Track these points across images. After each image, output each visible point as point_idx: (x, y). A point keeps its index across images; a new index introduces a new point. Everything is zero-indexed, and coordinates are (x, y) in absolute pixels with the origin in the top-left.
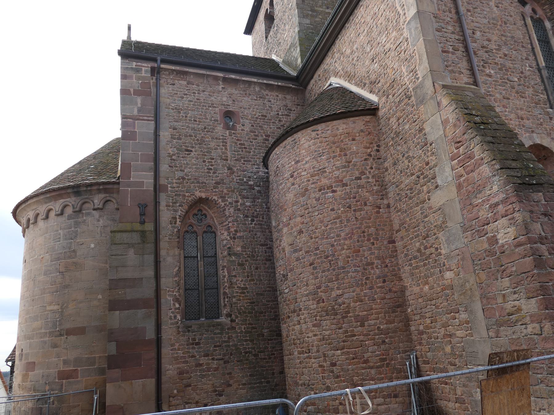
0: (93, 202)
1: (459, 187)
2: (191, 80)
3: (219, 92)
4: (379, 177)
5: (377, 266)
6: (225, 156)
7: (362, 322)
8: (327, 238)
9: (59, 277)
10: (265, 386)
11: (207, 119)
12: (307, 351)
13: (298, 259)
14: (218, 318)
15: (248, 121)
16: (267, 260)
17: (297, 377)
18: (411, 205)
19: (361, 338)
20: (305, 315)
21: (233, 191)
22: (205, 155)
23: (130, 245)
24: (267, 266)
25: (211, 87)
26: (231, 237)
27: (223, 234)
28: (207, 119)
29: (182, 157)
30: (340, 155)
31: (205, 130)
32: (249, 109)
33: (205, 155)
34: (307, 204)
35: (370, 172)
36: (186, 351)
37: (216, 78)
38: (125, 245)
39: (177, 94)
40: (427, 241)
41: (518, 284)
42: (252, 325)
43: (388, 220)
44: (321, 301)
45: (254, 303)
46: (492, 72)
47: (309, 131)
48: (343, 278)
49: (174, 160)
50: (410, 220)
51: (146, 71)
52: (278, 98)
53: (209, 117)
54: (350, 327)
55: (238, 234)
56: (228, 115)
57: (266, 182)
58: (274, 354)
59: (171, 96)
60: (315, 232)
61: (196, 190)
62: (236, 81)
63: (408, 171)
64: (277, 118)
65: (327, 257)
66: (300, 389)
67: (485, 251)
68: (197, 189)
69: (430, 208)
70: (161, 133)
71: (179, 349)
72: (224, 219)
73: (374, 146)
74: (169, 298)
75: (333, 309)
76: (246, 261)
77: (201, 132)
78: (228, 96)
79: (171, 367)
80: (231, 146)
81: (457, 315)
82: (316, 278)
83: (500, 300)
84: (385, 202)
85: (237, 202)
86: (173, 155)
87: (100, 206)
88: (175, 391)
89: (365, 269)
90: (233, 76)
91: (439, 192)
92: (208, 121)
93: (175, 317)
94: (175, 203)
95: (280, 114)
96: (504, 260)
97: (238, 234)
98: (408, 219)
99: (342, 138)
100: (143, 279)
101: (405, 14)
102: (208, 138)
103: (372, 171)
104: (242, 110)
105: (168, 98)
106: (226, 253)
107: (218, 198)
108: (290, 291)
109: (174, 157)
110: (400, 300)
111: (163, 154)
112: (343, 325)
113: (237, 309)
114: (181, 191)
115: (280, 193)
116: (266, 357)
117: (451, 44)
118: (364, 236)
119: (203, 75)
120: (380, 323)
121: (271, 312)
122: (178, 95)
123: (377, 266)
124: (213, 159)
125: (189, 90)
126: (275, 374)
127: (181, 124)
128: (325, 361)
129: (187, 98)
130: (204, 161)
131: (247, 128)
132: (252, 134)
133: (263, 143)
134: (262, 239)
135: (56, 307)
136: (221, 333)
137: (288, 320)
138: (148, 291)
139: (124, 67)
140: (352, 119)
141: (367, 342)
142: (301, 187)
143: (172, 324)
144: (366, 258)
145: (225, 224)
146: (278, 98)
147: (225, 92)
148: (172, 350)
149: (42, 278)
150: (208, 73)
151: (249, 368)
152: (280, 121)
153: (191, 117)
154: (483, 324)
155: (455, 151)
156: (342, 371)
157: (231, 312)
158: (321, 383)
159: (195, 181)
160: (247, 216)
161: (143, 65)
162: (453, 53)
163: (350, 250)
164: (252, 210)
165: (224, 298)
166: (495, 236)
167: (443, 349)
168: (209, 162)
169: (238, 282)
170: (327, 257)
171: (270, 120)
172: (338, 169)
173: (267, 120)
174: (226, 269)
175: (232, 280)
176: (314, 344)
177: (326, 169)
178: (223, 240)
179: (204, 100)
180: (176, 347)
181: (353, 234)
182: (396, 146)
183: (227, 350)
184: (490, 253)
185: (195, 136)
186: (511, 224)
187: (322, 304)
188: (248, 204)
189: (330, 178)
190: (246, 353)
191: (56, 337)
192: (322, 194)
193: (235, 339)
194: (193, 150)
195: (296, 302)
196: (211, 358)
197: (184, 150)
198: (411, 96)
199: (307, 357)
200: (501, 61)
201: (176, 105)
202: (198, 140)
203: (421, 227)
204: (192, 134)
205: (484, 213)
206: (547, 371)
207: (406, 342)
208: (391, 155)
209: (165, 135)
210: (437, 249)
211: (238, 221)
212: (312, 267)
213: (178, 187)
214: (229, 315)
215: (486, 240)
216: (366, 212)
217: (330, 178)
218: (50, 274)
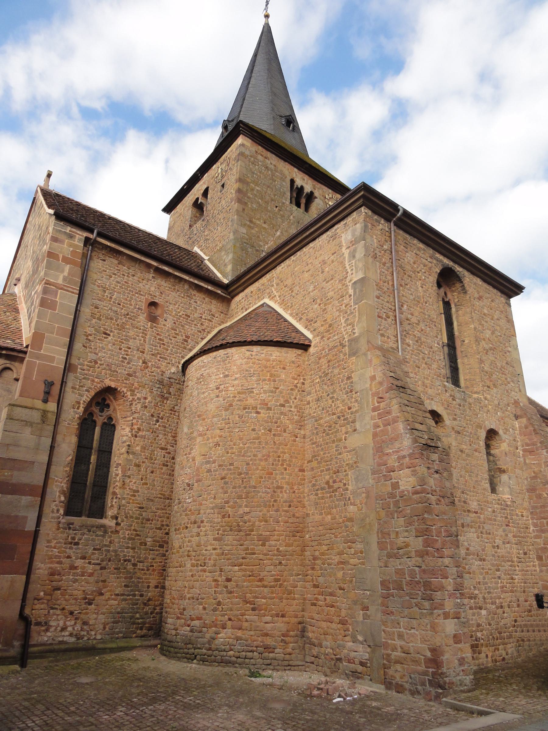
1: (375, 435)
4: (301, 408)
5: (285, 491)
6: (142, 348)
7: (264, 541)
8: (243, 456)
10: (138, 600)
11: (131, 305)
12: (203, 564)
13: (209, 471)
14: (102, 518)
15: (170, 317)
17: (184, 590)
18: (328, 441)
19: (261, 556)
20: (206, 527)
22: (123, 343)
23: (28, 423)
26: (132, 435)
27: (124, 429)
28: (131, 305)
29: (99, 339)
30: (269, 380)
32: (175, 305)
33: (123, 343)
34: (229, 418)
35: (293, 402)
36: (63, 551)
37: (149, 266)
38: (23, 423)
39: (106, 271)
40: (337, 476)
41: (410, 524)
42: (137, 531)
43: (302, 449)
44: (227, 516)
45: (143, 508)
46: (411, 342)
47: (243, 350)
48: (253, 497)
50: (324, 454)
51: (80, 240)
53: (133, 303)
54: (252, 544)
58: (153, 566)
60: (232, 448)
61: (107, 378)
62: (167, 275)
63: (330, 410)
64: (200, 321)
65: (240, 474)
66: (187, 603)
67: (388, 494)
69: (345, 447)
70: (82, 309)
71: (55, 548)
72: (129, 414)
73: (300, 379)
74: (55, 489)
75: (238, 526)
77: (123, 317)
79: (43, 565)
80: (150, 339)
81: (354, 545)
82: (226, 492)
84: (302, 432)
85: (145, 398)
88: (42, 594)
89: (274, 492)
90: (166, 269)
91: (356, 435)
93: (58, 511)
94: (82, 386)
95: (203, 317)
97: (140, 433)
98: (322, 453)
100: (35, 464)
101: (352, 274)
103: (295, 401)
104: (168, 304)
105: (96, 273)
106: (124, 450)
107: (127, 390)
108: (194, 501)
109: (89, 337)
110: (301, 525)
111: (80, 331)
112: (245, 543)
113: (125, 512)
115: (200, 401)
116: (145, 568)
117: (385, 311)
118: (279, 461)
120: (280, 544)
121: (158, 521)
122: (107, 273)
123: (285, 491)
124: (130, 348)
125: (119, 270)
126: (151, 587)
128: (221, 575)
129: (115, 278)
132: (173, 331)
133: (182, 343)
134: (163, 442)
136: (103, 536)
138: (39, 480)
141: (265, 561)
143: (52, 518)
144: (277, 481)
145: (128, 419)
148: (47, 547)
151: (125, 578)
153: (115, 299)
155: (377, 404)
156: (237, 587)
157: (118, 514)
158: (212, 597)
159: (107, 368)
162: (386, 320)
163: (263, 472)
166: (398, 482)
167: (335, 574)
168: (125, 351)
169: (131, 484)
170: (240, 474)
171: (193, 321)
172: (265, 392)
175: (125, 481)
176: (212, 557)
177: (254, 390)
178: (123, 436)
180: (53, 544)
181: (269, 456)
182: (322, 384)
183: (106, 555)
184: (392, 495)
186: (412, 475)
189: (256, 400)
190: (125, 561)
192: (247, 412)
193: (117, 544)
195: (199, 514)
196: (87, 561)
197: (102, 332)
198: (345, 346)
199: (201, 571)
200: (419, 334)
203: (333, 462)
206: (421, 596)
207: (300, 565)
208: (316, 391)
209: (86, 311)
210: (345, 485)
211: (143, 419)
212: (223, 481)
216: (285, 439)
217: (256, 400)
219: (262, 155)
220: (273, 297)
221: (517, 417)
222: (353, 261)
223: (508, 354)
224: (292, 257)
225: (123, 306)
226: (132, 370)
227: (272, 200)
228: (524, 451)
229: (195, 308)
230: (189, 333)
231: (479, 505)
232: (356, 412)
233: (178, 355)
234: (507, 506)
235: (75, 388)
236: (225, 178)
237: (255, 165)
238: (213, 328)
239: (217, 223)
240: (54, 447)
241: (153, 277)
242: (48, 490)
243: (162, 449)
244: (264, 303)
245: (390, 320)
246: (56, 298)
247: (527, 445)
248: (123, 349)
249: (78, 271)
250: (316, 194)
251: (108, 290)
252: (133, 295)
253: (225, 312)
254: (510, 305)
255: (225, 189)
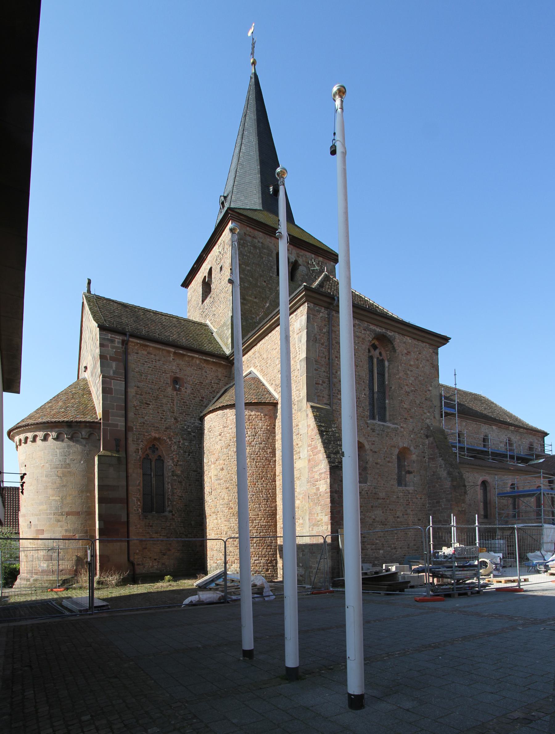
0: (81, 434)
1: (309, 461)
2: (150, 351)
3: (170, 362)
9: (58, 479)
11: (161, 382)
13: (219, 484)
14: (164, 512)
15: (189, 386)
16: (196, 481)
21: (177, 435)
22: (159, 408)
24: (196, 484)
25: (164, 358)
26: (174, 465)
28: (161, 382)
29: (143, 408)
31: (160, 390)
32: (191, 376)
33: (159, 408)
39: (140, 361)
49: (138, 410)
51: (118, 342)
52: (212, 370)
55: (179, 463)
56: (176, 381)
57: (199, 430)
59: (136, 362)
64: (211, 385)
68: (153, 431)
72: (170, 452)
74: (134, 499)
76: (183, 480)
78: (177, 366)
82: (230, 496)
83: (316, 515)
85: (179, 442)
86: (137, 406)
87: (87, 437)
88: (138, 551)
90: (181, 352)
92: (162, 383)
93: (138, 510)
95: (213, 382)
96: (320, 499)
97: (179, 463)
99: (253, 418)
101: (299, 354)
102: (161, 396)
105: (134, 364)
106: (170, 474)
107: (167, 438)
109: (137, 408)
111: (130, 404)
114: (142, 431)
115: (211, 443)
117: (322, 379)
119: (159, 349)
122: (141, 362)
125: (149, 358)
127: (142, 384)
129: (147, 364)
130: (158, 413)
131: (189, 391)
132: (192, 395)
133: (200, 403)
135: (57, 498)
137: (210, 517)
139: (102, 338)
140: (261, 406)
142: (225, 443)
146: (212, 370)
147: (174, 362)
148: (136, 528)
149: (44, 478)
150: (163, 348)
152: (212, 387)
154: (308, 525)
155: (311, 443)
159: (152, 426)
160: (185, 452)
161: (116, 337)
162: (322, 385)
164: (189, 448)
165: (168, 501)
168: (161, 413)
171: (206, 386)
173: (203, 386)
174: (170, 484)
175: (174, 491)
179: (159, 367)
184: (316, 494)
185: (152, 394)
187: (231, 510)
188: (186, 444)
191: (58, 516)
194: (151, 403)
198: (295, 404)
201: (140, 370)
202: (154, 397)
204: (150, 392)
205: (317, 476)
209: (132, 391)
211: (179, 455)
213: (140, 429)
214: (171, 511)
215: (315, 488)
218: (51, 477)
219: (250, 236)
220: (256, 367)
221: (427, 437)
222: (300, 345)
223: (428, 392)
224: (266, 337)
225: (156, 383)
226: (168, 425)
227: (261, 276)
228: (429, 459)
229: (206, 376)
230: (204, 395)
231: (386, 494)
232: (301, 447)
233: (198, 411)
234: (409, 493)
235: (134, 441)
236: (223, 261)
237: (245, 247)
238: (220, 389)
239: (220, 302)
240: (129, 476)
241: (173, 359)
242: (130, 500)
243: (194, 471)
244: (251, 371)
245: (325, 385)
246: (111, 386)
247: (431, 455)
248: (160, 412)
249: (122, 365)
250: (300, 261)
251: (143, 374)
252: (161, 374)
253: (229, 376)
254: (437, 354)
255: (223, 272)
